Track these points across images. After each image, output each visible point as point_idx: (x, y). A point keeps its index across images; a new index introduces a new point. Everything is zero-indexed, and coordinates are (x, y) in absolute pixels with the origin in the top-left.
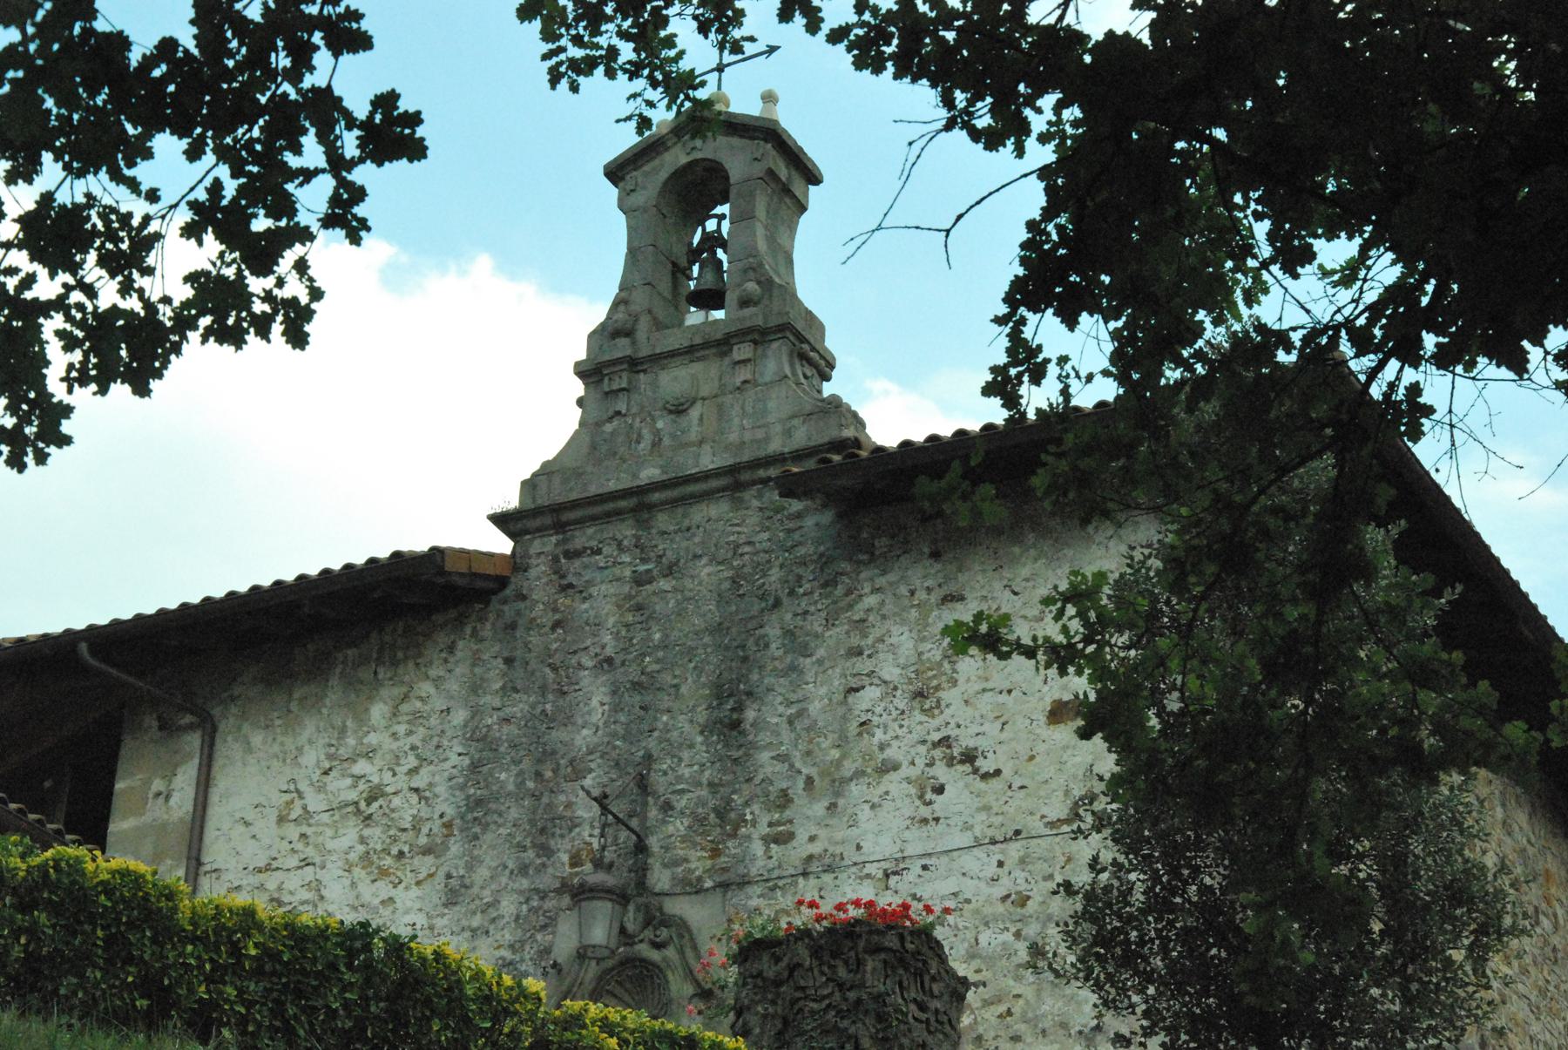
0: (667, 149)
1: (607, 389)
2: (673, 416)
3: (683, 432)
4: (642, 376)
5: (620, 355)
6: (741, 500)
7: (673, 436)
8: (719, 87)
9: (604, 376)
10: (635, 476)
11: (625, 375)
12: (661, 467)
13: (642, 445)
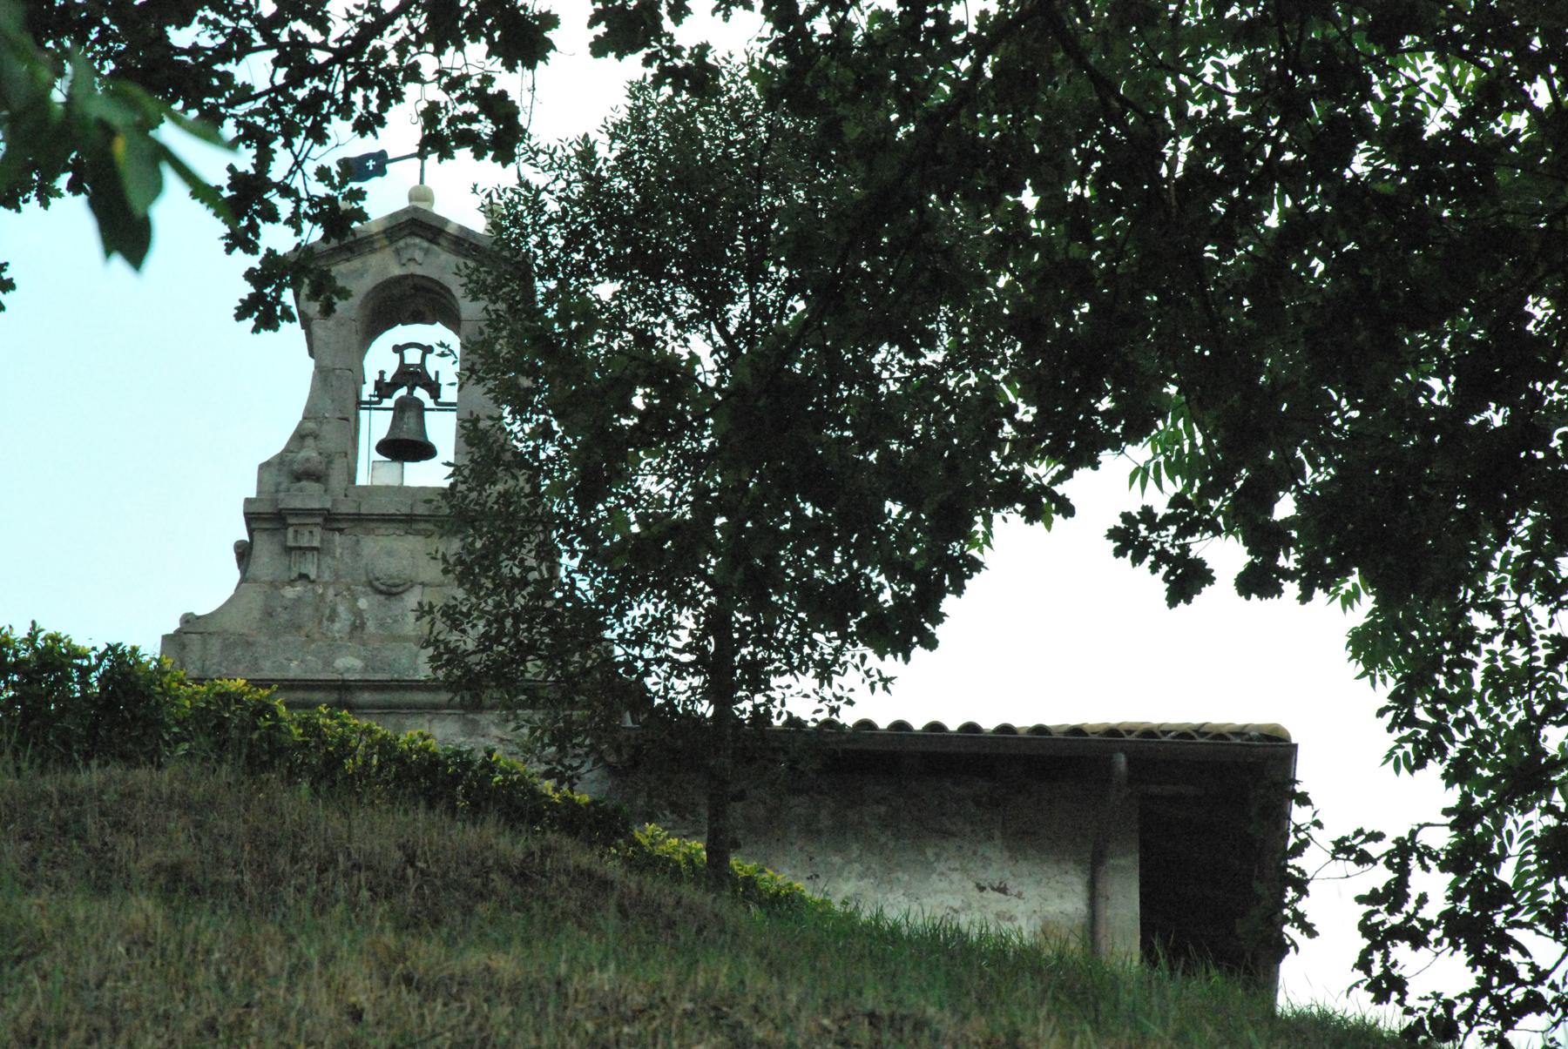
0: (373, 251)
1: (291, 543)
2: (382, 598)
3: (395, 621)
4: (337, 536)
5: (317, 505)
6: (475, 723)
7: (382, 625)
8: (422, 181)
9: (287, 526)
10: (328, 663)
11: (317, 531)
12: (364, 658)
13: (337, 626)
